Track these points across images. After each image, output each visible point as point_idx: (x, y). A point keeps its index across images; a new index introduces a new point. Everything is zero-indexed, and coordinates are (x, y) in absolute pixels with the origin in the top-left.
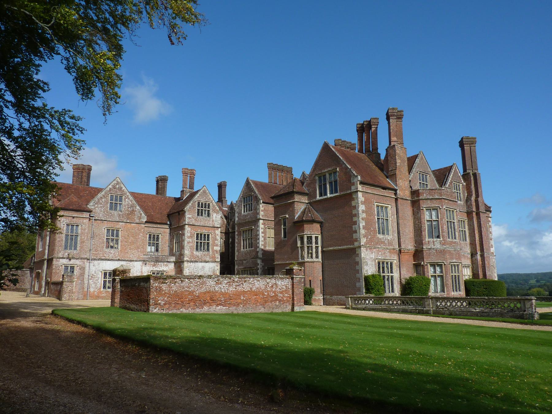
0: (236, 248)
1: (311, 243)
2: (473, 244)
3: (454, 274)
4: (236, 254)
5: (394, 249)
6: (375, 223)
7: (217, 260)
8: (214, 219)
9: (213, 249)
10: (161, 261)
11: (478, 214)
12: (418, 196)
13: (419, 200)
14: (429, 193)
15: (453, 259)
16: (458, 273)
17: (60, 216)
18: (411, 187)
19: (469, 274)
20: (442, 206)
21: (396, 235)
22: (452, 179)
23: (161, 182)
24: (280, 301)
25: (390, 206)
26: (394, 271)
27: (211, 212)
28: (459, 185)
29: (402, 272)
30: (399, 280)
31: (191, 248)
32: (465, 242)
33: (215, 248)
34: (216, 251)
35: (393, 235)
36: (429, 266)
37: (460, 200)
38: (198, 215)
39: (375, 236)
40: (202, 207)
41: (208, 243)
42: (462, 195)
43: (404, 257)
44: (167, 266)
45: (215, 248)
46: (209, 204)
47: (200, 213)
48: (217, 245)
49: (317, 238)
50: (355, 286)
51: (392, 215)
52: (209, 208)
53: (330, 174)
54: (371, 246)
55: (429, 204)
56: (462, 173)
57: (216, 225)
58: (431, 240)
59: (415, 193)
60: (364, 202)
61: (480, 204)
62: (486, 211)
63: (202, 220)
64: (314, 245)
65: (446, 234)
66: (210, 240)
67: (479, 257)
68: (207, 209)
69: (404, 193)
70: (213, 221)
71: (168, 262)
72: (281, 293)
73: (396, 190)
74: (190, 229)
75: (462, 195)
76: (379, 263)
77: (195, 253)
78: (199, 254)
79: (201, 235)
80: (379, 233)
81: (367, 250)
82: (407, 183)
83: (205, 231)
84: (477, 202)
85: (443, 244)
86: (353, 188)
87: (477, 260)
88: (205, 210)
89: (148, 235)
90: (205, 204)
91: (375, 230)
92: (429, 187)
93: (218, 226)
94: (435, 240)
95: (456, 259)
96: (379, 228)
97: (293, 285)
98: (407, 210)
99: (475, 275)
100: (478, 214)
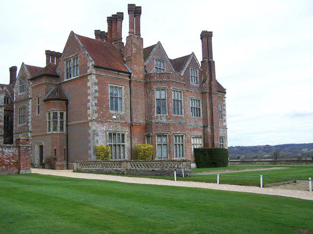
0: (14, 124)
1: (56, 118)
2: (205, 119)
3: (178, 143)
4: (14, 128)
5: (126, 123)
15: (177, 131)
16: (182, 142)
17: (213, 144)
19: (200, 143)
20: (169, 87)
21: (129, 111)
24: (6, 166)
25: (124, 87)
26: (125, 141)
29: (133, 142)
30: (130, 147)
32: (198, 117)
37: (197, 83)
42: (198, 79)
43: (136, 130)
49: (62, 114)
50: (88, 153)
51: (126, 94)
54: (101, 120)
58: (159, 115)
59: (147, 76)
60: (98, 83)
64: (59, 120)
65: (171, 111)
67: (209, 130)
72: (8, 159)
73: (130, 74)
75: (198, 79)
82: (142, 68)
84: (210, 83)
86: (89, 71)
91: (107, 107)
94: (162, 115)
95: (180, 131)
96: (112, 106)
97: (19, 152)
98: (140, 91)
99: (205, 143)
100: (210, 94)
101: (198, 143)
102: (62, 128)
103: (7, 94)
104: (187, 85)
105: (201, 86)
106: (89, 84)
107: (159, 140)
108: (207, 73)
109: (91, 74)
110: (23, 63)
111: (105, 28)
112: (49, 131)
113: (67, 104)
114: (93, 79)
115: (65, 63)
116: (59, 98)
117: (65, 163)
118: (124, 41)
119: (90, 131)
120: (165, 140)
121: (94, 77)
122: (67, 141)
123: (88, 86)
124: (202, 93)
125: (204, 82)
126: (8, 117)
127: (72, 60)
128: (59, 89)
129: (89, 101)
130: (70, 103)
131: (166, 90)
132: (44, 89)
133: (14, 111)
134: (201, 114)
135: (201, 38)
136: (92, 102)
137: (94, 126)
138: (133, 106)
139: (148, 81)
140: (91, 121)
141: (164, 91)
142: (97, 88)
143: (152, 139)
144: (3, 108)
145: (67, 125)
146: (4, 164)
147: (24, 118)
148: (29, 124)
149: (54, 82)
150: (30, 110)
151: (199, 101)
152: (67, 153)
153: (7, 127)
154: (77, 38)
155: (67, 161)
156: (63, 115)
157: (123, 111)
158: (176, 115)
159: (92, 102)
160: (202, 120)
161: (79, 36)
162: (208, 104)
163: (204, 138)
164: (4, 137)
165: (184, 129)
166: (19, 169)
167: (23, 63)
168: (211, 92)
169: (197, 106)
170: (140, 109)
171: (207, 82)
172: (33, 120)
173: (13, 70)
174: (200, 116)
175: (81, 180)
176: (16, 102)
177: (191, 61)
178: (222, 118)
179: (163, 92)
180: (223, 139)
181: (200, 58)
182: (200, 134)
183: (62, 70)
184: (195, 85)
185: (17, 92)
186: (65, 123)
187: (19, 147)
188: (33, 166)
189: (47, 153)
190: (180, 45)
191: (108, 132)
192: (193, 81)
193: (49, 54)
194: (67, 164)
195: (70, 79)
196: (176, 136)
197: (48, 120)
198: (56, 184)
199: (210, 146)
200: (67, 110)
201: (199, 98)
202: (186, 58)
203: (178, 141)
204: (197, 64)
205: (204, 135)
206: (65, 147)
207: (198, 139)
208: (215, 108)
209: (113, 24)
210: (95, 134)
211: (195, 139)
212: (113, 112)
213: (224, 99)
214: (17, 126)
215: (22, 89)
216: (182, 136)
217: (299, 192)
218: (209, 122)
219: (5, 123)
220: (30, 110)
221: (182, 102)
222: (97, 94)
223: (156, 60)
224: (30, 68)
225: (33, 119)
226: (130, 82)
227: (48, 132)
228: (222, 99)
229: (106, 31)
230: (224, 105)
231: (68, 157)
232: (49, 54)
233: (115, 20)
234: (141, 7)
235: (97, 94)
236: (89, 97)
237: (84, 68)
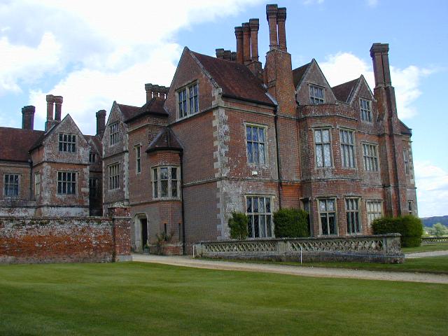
0: (103, 189)
2: (385, 174)
3: (351, 210)
4: (104, 196)
6: (244, 149)
7: (86, 204)
8: (81, 154)
9: (80, 190)
10: (20, 207)
11: (391, 136)
12: (306, 111)
13: (305, 119)
14: (318, 110)
17: (399, 212)
18: (297, 103)
19: (380, 211)
20: (335, 126)
21: (275, 163)
22: (358, 94)
23: (29, 112)
24: (95, 249)
25: (266, 126)
27: (77, 146)
28: (368, 103)
31: (52, 190)
33: (83, 190)
34: (84, 193)
35: (270, 163)
36: (318, 201)
38: (61, 149)
40: (65, 140)
41: (74, 184)
42: (372, 115)
44: (25, 211)
45: (83, 190)
46: (74, 137)
47: (62, 147)
48: (85, 187)
52: (74, 141)
53: (190, 88)
55: (319, 123)
56: (374, 87)
57: (84, 162)
59: (301, 109)
61: (394, 126)
62: (402, 133)
63: (65, 157)
66: (77, 180)
67: (392, 190)
68: (72, 142)
69: (287, 110)
70: (79, 157)
71: (27, 207)
74: (50, 167)
75: (372, 115)
77: (56, 195)
78: (62, 197)
79: (65, 174)
80: (251, 161)
81: (231, 183)
83: (69, 169)
84: (389, 120)
86: (214, 104)
87: (389, 193)
88: (69, 144)
89: (4, 176)
90: (70, 136)
92: (324, 102)
93: (87, 163)
95: (354, 192)
98: (291, 131)
99: (387, 211)
100: (391, 136)
101: (376, 210)
102: (174, 193)
103: (92, 148)
104: (356, 120)
105: (376, 125)
106: (215, 123)
107: (323, 207)
108: (385, 104)
109: (217, 108)
110: (115, 102)
111: (231, 46)
112: (156, 196)
113: (181, 155)
114: (221, 114)
115: (177, 94)
116: (168, 147)
117: (180, 245)
118: (262, 59)
119: (219, 196)
120: (331, 206)
121: (222, 112)
122: (183, 212)
123: (214, 125)
124: (379, 136)
125: (380, 119)
126: (94, 181)
127: (187, 90)
128: (168, 135)
129: (216, 149)
130: (186, 153)
131: (330, 130)
132: (148, 136)
133: (104, 170)
134: (379, 168)
135: (372, 55)
136: (221, 151)
137: (225, 187)
138: (281, 156)
139: (302, 120)
140: (221, 179)
141: (327, 132)
142: (227, 128)
143: (312, 205)
144: (88, 167)
145: (182, 187)
147: (117, 182)
148: (125, 189)
149: (161, 123)
150: (126, 168)
151: (374, 147)
152: (184, 229)
153: (94, 195)
154: (194, 57)
155: (184, 242)
156: (175, 171)
159: (221, 151)
160: (380, 176)
161: (196, 54)
162: (388, 151)
163: (385, 203)
164: (91, 210)
165: (358, 190)
166: (114, 255)
167: (115, 102)
168: (392, 138)
169: (372, 154)
170: (293, 159)
171: (385, 118)
172: (132, 182)
173: (100, 115)
174: (377, 170)
175: (312, 261)
176: (105, 159)
177: (361, 87)
178: (408, 172)
179: (325, 133)
180: (412, 203)
181: (372, 84)
182: (379, 196)
183: (172, 104)
184: (368, 123)
185: (108, 146)
186: (179, 184)
187: (114, 220)
188: (133, 250)
189: (154, 228)
190: (344, 67)
191: (245, 196)
192: (365, 118)
193: (151, 89)
194: (184, 246)
195: (185, 117)
196: (347, 200)
197: (153, 180)
199: (394, 217)
200: (181, 164)
201: (375, 140)
202: (353, 83)
203: (350, 208)
204: (369, 92)
205: (385, 198)
206: (180, 221)
207: (375, 206)
208: (398, 156)
209: (244, 36)
210: (227, 198)
211: (372, 205)
213: (409, 144)
214: (108, 192)
215: (113, 136)
216: (356, 200)
218: (391, 177)
219: (90, 189)
220: (126, 168)
221: (354, 148)
222: (228, 138)
223: (311, 87)
224: (125, 109)
225: (131, 179)
226: (276, 118)
227: (154, 199)
228: (407, 145)
229: (233, 49)
230: (411, 153)
231: (184, 236)
232: (151, 89)
233: (246, 32)
234: (285, 9)
235: (228, 138)
236: (216, 143)
237: (208, 97)
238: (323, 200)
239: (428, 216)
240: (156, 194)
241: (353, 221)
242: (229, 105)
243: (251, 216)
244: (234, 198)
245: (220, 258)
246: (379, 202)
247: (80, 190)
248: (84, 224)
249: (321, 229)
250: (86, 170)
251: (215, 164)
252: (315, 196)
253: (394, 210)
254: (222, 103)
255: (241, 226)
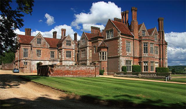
2: (160, 55)
9: (72, 56)
11: (162, 45)
17: (163, 66)
18: (139, 35)
21: (133, 52)
32: (151, 54)
33: (73, 56)
39: (125, 52)
49: (106, 53)
58: (145, 54)
63: (68, 47)
64: (105, 55)
65: (150, 52)
69: (136, 37)
72: (92, 71)
76: (126, 61)
78: (67, 58)
85: (149, 55)
91: (125, 50)
98: (137, 43)
99: (160, 65)
102: (106, 59)
146: (90, 73)
155: (108, 72)
157: (131, 52)
158: (151, 54)
166: (96, 76)
198: (95, 81)
201: (158, 46)
206: (107, 66)
212: (127, 52)
217: (153, 87)
229: (120, 17)
238: (145, 62)
239: (139, 55)
240: (101, 59)
241: (152, 67)
242: (122, 36)
243: (126, 66)
244: (123, 61)
245: (120, 77)
246: (158, 63)
247: (72, 56)
248: (89, 67)
249: (144, 70)
250: (74, 51)
251: (118, 52)
252: (142, 61)
253: (162, 65)
254: (121, 36)
255: (124, 69)
